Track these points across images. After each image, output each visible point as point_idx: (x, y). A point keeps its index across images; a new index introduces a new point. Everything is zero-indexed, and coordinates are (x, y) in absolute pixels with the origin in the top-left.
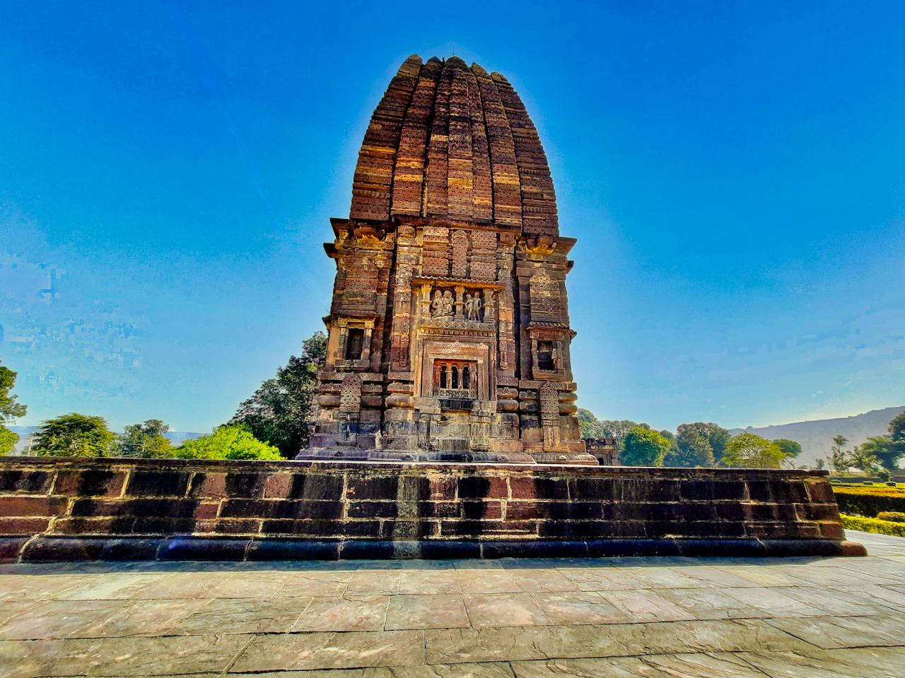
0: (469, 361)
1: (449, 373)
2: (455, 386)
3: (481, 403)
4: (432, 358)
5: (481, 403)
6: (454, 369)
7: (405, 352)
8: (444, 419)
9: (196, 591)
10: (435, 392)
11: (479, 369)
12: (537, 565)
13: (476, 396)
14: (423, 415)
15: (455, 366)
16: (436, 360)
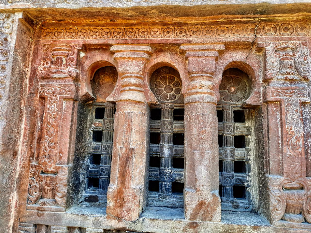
1: (131, 100)
15: (165, 58)
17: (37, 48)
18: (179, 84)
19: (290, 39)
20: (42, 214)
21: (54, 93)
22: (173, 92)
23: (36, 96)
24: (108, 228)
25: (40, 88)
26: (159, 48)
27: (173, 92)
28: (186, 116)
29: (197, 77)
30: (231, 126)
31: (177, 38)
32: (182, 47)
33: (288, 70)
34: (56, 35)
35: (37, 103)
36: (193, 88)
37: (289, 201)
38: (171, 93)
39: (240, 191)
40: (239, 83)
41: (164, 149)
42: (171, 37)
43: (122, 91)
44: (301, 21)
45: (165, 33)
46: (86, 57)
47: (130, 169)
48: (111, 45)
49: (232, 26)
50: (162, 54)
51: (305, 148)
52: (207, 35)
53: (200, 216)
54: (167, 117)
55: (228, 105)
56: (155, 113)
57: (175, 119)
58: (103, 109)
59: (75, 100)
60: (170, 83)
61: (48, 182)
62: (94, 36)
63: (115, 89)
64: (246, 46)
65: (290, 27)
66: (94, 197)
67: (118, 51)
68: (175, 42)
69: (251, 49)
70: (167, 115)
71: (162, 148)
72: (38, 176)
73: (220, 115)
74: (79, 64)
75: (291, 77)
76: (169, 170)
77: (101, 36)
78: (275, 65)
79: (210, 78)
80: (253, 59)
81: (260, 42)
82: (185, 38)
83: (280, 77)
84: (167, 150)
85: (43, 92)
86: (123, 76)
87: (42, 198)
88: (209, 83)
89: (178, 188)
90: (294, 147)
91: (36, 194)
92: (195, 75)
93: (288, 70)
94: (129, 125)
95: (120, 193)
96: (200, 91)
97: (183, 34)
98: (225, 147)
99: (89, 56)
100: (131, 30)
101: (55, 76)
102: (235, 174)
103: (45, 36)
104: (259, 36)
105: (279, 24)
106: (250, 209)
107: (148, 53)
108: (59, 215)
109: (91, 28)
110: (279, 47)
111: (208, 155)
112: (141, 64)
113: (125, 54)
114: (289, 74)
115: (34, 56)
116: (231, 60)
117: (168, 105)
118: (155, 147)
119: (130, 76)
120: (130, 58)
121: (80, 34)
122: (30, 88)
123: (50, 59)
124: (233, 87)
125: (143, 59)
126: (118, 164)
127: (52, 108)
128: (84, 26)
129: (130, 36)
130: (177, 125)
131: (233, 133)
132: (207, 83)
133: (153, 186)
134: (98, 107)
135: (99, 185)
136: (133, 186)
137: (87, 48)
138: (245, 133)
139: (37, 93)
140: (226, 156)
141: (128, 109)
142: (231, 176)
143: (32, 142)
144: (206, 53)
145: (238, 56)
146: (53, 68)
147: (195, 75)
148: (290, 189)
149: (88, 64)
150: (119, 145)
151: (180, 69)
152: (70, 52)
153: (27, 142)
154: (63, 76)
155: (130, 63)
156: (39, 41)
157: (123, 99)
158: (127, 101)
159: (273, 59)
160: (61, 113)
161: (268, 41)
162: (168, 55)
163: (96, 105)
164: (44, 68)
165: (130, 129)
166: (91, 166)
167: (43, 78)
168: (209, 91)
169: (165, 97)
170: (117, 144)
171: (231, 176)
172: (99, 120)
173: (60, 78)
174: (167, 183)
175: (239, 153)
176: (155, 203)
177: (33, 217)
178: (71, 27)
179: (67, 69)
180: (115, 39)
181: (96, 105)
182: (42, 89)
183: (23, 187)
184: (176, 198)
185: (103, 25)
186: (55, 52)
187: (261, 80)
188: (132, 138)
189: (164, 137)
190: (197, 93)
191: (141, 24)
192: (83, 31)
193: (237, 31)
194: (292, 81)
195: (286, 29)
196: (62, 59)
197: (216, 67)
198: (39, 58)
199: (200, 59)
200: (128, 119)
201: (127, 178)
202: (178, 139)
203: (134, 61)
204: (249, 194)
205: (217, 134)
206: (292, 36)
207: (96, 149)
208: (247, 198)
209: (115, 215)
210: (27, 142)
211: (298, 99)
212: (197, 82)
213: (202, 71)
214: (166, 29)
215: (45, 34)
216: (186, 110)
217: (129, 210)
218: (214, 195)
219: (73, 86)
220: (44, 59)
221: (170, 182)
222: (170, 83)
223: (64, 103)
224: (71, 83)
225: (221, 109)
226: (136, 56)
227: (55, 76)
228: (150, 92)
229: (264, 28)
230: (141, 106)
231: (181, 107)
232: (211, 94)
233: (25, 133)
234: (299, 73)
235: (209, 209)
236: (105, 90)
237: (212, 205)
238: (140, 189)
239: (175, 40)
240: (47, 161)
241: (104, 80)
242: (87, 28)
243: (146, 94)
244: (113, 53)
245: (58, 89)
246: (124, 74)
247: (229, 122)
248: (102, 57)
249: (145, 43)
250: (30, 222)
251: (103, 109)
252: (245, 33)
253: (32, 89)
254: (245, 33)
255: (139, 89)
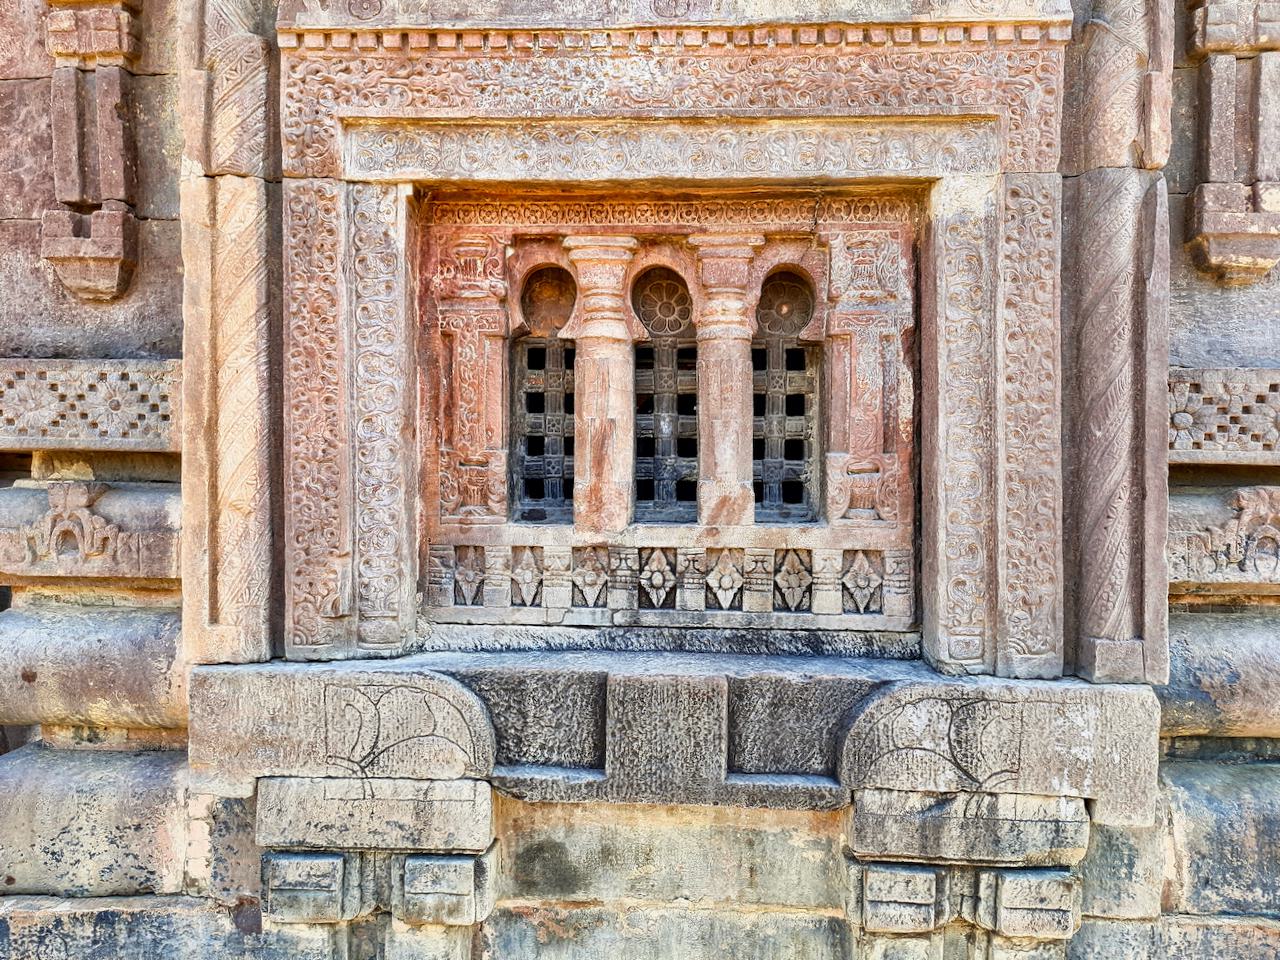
0: (817, 195)
1: (604, 337)
2: (665, 482)
3: (963, 709)
4: (372, 180)
5: (963, 709)
6: (655, 289)
7: (105, 102)
8: (543, 867)
9: (980, 132)
10: (448, 569)
11: (951, 280)
12: (779, 185)
13: (897, 603)
14: (293, 870)
15: (661, 257)
16: (433, 202)
17: (428, 241)
18: (685, 300)
19: (872, 227)
20: (469, 530)
21: (467, 325)
22: (675, 316)
23: (436, 332)
24: (580, 545)
25: (440, 317)
26: (649, 241)
27: (675, 316)
28: (701, 362)
29: (717, 293)
30: (780, 377)
31: (681, 223)
32: (691, 239)
33: (866, 282)
34: (461, 215)
35: (438, 344)
36: (711, 314)
37: (857, 490)
38: (672, 318)
39: (793, 491)
40: (796, 296)
41: (662, 423)
42: (672, 222)
43: (586, 320)
44: (890, 195)
45: (662, 214)
46: (516, 257)
47: (610, 452)
48: (565, 236)
49: (776, 201)
50: (656, 250)
51: (884, 408)
52: (735, 218)
53: (722, 519)
54: (665, 363)
55: (775, 339)
56: (644, 356)
57: (681, 366)
58: (543, 351)
59: (504, 339)
60: (670, 296)
61: (474, 479)
62: (533, 218)
63: (573, 315)
64: (803, 238)
65: (873, 204)
66: (538, 511)
67: (577, 247)
68: (679, 231)
69: (811, 241)
70: (665, 359)
71: (658, 420)
72: (455, 469)
73: (759, 359)
74: (507, 272)
75: (869, 293)
76: (671, 460)
77: (545, 218)
78: (844, 273)
79: (740, 296)
80: (813, 259)
81: (823, 233)
82: (696, 223)
83: (853, 292)
84: (666, 425)
85: (448, 324)
86: (589, 293)
87: (463, 504)
88: (738, 305)
89: (687, 491)
90: (867, 408)
91: (455, 498)
92: (714, 290)
93: (866, 282)
94: (604, 380)
95: (595, 492)
96: (722, 318)
97: (693, 215)
98: (769, 416)
99: (521, 253)
100: (600, 208)
101: (466, 294)
102: (786, 462)
103: (440, 219)
104: (820, 221)
105: (856, 199)
106: (809, 518)
107: (631, 249)
108: (498, 529)
109: (526, 204)
110: (854, 240)
111: (734, 426)
112: (619, 271)
113: (590, 253)
114: (866, 288)
115: (423, 256)
116: (776, 261)
117: (667, 340)
118: (647, 420)
119: (602, 294)
120: (599, 260)
121: (505, 214)
122: (421, 316)
123: (453, 263)
124: (785, 303)
125: (623, 262)
126: (588, 446)
127: (465, 352)
128: (512, 200)
129: (598, 218)
130: (683, 377)
131: (783, 390)
132: (735, 305)
133: (644, 489)
134: (531, 346)
135: (546, 492)
136: (616, 478)
137: (519, 240)
138: (804, 389)
139: (437, 326)
140: (771, 431)
141: (603, 352)
142: (777, 465)
143: (437, 414)
144: (733, 251)
145: (787, 255)
146: (461, 280)
147: (714, 290)
148: (859, 472)
149: (521, 269)
150: (589, 414)
151: (688, 276)
152: (490, 249)
153: (428, 414)
154: (480, 295)
155: (599, 269)
156: (429, 227)
157: (589, 335)
158: (598, 338)
159: (841, 263)
160: (483, 363)
161: (834, 231)
162: (667, 251)
163: (527, 343)
164: (444, 280)
165: (605, 388)
166: (528, 458)
167: (443, 299)
168: (737, 318)
169: (661, 325)
170: (584, 413)
171: (777, 465)
172: (536, 372)
173: (474, 299)
174: (667, 483)
175: (793, 424)
176: (648, 516)
177: (453, 535)
178: (488, 200)
179: (487, 282)
180: (572, 223)
181: (527, 343)
182: (444, 319)
183: (431, 488)
184: (684, 507)
185: (548, 198)
186: (462, 249)
187: (824, 297)
188: (610, 404)
189: (660, 400)
190: (717, 322)
191: (616, 196)
192: (512, 209)
193: (786, 211)
194: (872, 300)
195: (866, 209)
196: (475, 261)
197: (750, 274)
198: (433, 260)
199: (722, 262)
200: (601, 371)
201: (606, 467)
202: (687, 404)
203: (607, 266)
204: (809, 494)
205: (751, 392)
206: (875, 221)
207: (535, 426)
208: (805, 501)
209: (588, 524)
210: (428, 414)
211: (878, 330)
212: (716, 304)
213: (726, 283)
214: (663, 205)
215: (439, 215)
216: (700, 352)
217: (611, 516)
218: (743, 486)
219: (502, 313)
220: (442, 263)
221: (673, 480)
222: (670, 296)
223: (487, 342)
224: (496, 307)
225: (764, 347)
226: (610, 257)
227: (466, 294)
228: (636, 320)
229: (830, 205)
230: (623, 346)
231: (469, 657)
232: (741, 323)
233: (422, 398)
234: (883, 287)
235: (736, 507)
236: (543, 313)
237: (740, 502)
238: (628, 483)
239: (680, 227)
240: (468, 444)
241: (540, 293)
242: (518, 203)
243: (629, 324)
244: (568, 250)
245: (475, 319)
246: (589, 289)
247: (777, 370)
248: (547, 257)
249: (626, 230)
250: (449, 543)
251: (543, 351)
252: (798, 215)
253: (425, 319)
254: (798, 215)
255: (616, 316)
